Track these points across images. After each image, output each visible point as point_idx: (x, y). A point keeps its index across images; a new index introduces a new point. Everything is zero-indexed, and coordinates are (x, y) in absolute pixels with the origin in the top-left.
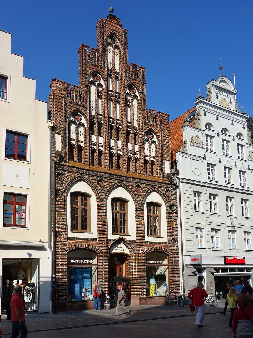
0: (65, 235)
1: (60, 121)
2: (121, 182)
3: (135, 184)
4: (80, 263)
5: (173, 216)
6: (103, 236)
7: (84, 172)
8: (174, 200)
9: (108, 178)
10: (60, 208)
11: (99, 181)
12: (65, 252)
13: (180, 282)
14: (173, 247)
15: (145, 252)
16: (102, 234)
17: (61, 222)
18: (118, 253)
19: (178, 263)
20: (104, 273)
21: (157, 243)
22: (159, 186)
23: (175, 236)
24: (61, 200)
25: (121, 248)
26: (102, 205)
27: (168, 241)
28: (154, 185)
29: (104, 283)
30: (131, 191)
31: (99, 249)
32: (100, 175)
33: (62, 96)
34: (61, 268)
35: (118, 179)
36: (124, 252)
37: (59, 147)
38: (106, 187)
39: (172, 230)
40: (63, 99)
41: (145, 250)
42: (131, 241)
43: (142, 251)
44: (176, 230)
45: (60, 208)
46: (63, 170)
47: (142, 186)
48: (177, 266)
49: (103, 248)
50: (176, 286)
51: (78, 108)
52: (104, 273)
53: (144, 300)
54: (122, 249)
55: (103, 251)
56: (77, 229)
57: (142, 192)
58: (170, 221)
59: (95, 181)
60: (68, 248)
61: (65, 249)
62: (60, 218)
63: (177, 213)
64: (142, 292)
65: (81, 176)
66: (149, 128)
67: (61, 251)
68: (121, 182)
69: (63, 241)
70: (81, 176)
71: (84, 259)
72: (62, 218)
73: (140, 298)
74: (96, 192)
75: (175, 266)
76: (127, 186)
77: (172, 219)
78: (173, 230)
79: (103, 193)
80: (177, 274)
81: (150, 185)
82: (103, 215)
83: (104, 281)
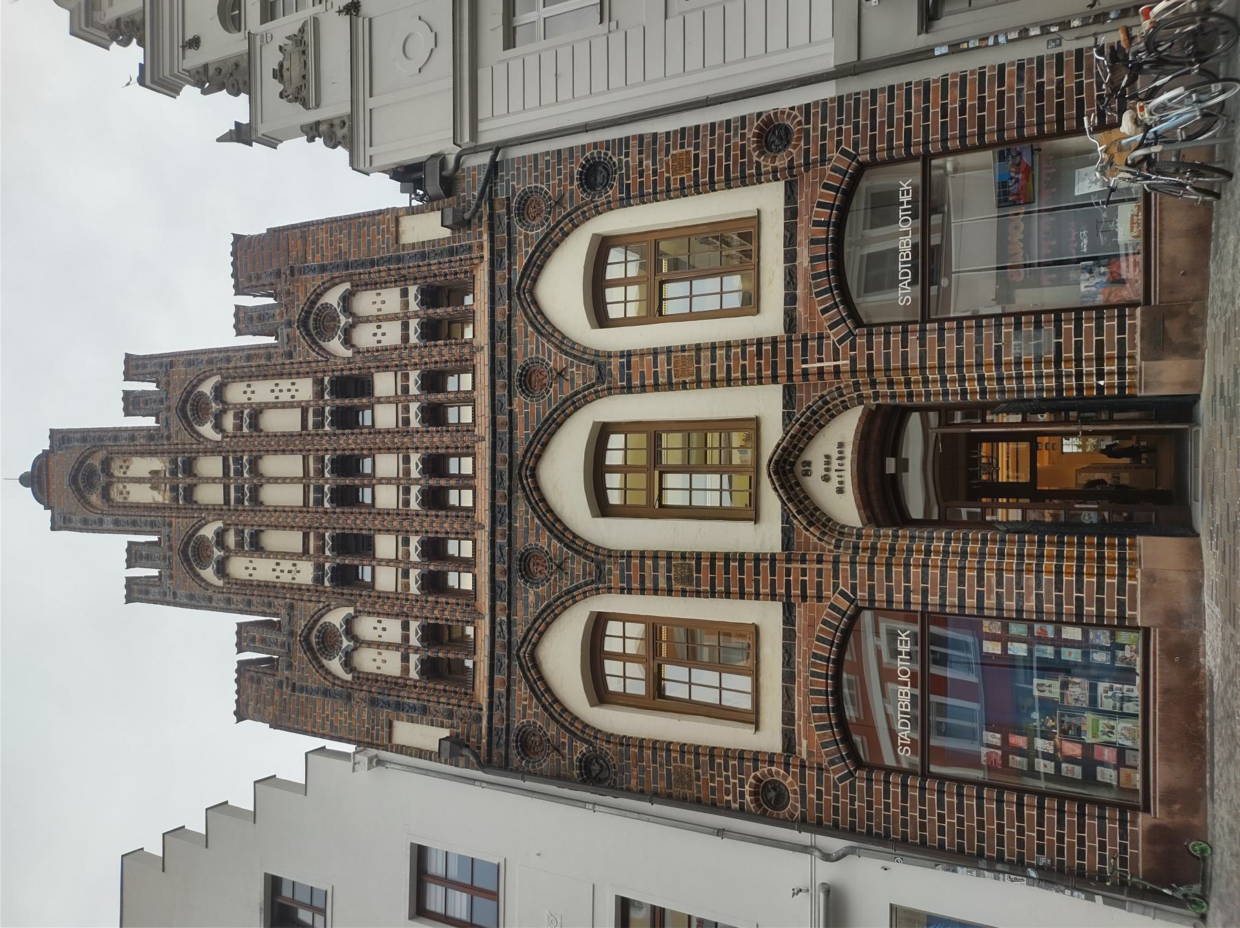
0: (774, 769)
1: (350, 715)
2: (520, 474)
3: (519, 399)
6: (765, 577)
11: (528, 576)
12: (852, 785)
14: (807, 142)
15: (842, 330)
16: (757, 582)
17: (712, 776)
18: (862, 433)
19: (908, 91)
20: (971, 586)
21: (790, 256)
23: (743, 135)
26: (622, 571)
27: (777, 180)
28: (510, 298)
29: (1029, 587)
31: (833, 607)
32: (503, 387)
34: (941, 818)
37: (429, 736)
38: (549, 546)
41: (833, 336)
42: (788, 417)
43: (836, 351)
48: (927, 99)
49: (827, 580)
50: (1070, 84)
52: (971, 586)
54: (835, 455)
58: (668, 179)
59: (531, 598)
60: (832, 763)
61: (841, 779)
67: (853, 800)
68: (520, 474)
69: (803, 780)
70: (518, 657)
72: (697, 767)
74: (574, 404)
75: (926, 110)
77: (655, 172)
78: (712, 153)
80: (982, 90)
82: (669, 570)
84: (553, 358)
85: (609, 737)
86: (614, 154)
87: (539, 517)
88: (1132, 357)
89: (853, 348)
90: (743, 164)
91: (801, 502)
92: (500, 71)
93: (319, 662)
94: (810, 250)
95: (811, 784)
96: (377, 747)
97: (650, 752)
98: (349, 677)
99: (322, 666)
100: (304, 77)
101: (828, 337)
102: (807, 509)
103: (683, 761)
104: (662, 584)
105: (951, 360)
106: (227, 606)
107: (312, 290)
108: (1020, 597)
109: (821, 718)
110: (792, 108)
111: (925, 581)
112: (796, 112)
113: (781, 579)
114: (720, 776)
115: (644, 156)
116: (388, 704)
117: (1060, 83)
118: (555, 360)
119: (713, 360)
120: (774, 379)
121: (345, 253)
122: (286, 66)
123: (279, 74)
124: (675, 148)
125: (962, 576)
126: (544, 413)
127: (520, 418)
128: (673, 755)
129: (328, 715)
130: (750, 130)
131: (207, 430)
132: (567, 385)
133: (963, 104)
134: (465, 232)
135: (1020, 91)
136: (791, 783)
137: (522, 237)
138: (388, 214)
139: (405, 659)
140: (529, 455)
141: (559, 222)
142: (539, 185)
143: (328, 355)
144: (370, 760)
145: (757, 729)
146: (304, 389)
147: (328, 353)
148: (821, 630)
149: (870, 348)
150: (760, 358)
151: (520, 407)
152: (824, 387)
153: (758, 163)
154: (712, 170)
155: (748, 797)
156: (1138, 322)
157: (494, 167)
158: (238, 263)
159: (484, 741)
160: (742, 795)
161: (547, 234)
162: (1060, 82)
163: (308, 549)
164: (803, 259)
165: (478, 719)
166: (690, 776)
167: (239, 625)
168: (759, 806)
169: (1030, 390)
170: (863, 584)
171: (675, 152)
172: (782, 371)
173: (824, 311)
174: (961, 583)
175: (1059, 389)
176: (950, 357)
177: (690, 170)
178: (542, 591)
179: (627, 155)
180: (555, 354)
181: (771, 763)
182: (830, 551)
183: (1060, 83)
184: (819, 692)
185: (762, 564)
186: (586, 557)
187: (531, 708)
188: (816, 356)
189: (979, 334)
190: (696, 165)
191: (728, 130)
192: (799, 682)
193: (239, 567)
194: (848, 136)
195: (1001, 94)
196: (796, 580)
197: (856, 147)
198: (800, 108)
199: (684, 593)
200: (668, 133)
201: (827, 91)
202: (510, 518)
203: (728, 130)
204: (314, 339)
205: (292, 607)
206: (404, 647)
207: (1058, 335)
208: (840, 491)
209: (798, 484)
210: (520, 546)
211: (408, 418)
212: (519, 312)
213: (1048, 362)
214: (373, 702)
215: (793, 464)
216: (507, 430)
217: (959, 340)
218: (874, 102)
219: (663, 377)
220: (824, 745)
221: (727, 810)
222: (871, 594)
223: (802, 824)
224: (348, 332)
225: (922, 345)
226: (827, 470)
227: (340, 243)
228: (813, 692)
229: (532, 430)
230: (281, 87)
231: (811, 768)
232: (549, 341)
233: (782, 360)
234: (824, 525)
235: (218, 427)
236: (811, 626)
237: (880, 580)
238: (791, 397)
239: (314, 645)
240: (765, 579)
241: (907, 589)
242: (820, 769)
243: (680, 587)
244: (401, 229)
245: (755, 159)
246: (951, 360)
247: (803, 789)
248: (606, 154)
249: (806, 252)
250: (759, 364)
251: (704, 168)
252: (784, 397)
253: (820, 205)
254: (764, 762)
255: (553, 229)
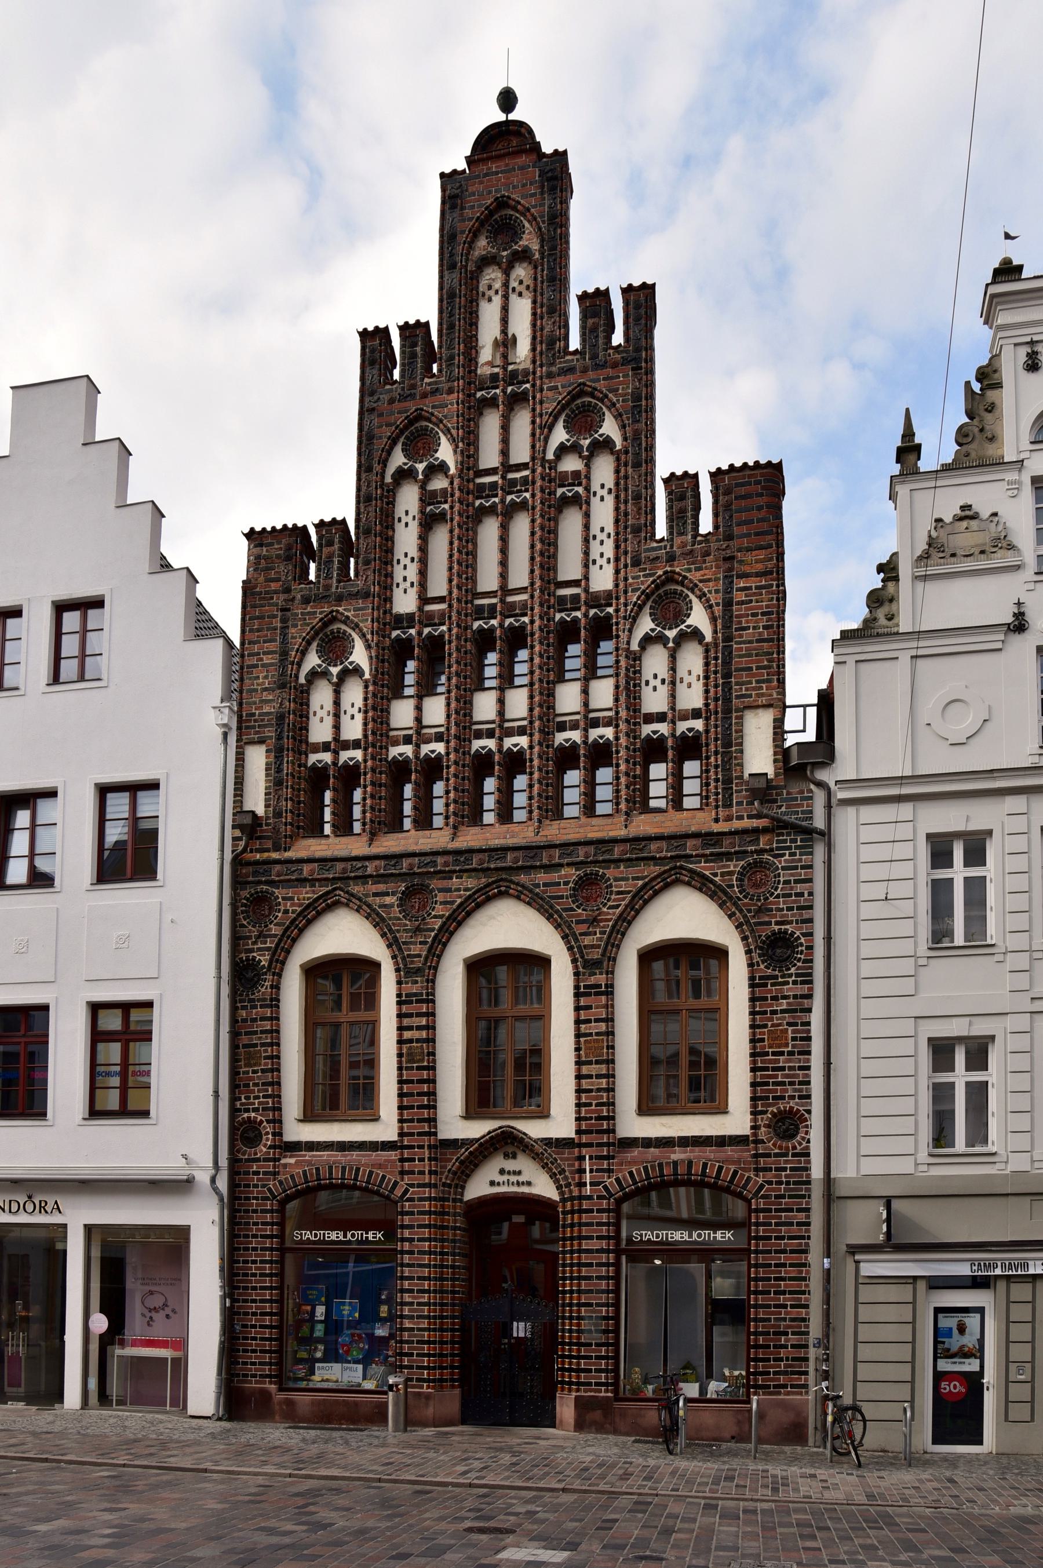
0: (270, 1136)
1: (266, 689)
2: (502, 880)
3: (572, 874)
4: (333, 1242)
5: (785, 997)
6: (417, 1128)
7: (344, 870)
8: (790, 909)
9: (447, 875)
10: (256, 1033)
11: (406, 897)
12: (267, 1199)
13: (807, 1333)
16: (412, 1121)
19: (803, 1238)
21: (685, 1142)
22: (703, 855)
23: (792, 1097)
24: (258, 1000)
25: (519, 1173)
26: (415, 995)
29: (418, 1323)
30: (552, 907)
31: (396, 1183)
33: (274, 586)
35: (489, 869)
36: (536, 1190)
37: (256, 802)
38: (435, 917)
39: (774, 1069)
40: (278, 599)
41: (610, 1181)
42: (548, 1142)
43: (598, 1184)
44: (801, 1068)
45: (256, 1033)
46: (267, 883)
47: (610, 873)
48: (792, 1252)
49: (416, 1179)
51: (332, 611)
52: (417, 1285)
53: (599, 1412)
54: (521, 1179)
55: (768, 1190)
56: (334, 1105)
57: (610, 903)
58: (765, 1026)
59: (388, 900)
60: (281, 1183)
61: (270, 1190)
62: (254, 1072)
63: (807, 979)
64: (590, 1371)
65: (335, 889)
66: (660, 572)
67: (256, 1198)
68: (502, 880)
69: (265, 1160)
70: (335, 889)
71: (344, 1226)
72: (263, 1071)
73: (576, 1397)
75: (784, 1251)
76: (531, 891)
77: (774, 1012)
78: (783, 1069)
79: (421, 943)
80: (791, 1293)
81: (653, 858)
82: (418, 1041)
83: (419, 1317)
84: (610, 911)
85: (276, 987)
86: (799, 968)
87: (461, 904)
88: (578, 1390)
89: (599, 1197)
90: (767, 1098)
91: (481, 1153)
92: (904, 831)
93: (313, 639)
94: (683, 1161)
95: (263, 1167)
96: (239, 728)
97: (269, 1028)
98: (302, 680)
99: (309, 643)
100: (953, 555)
101: (609, 1177)
102: (476, 1157)
103: (266, 1058)
104: (407, 1035)
105: (584, 1271)
106: (363, 499)
107: (706, 590)
108: (412, 1317)
109: (311, 1175)
110: (809, 1141)
111: (419, 1252)
112: (804, 1144)
113: (415, 1141)
114: (259, 1091)
115: (791, 1000)
116: (279, 738)
117: (785, 1347)
118: (608, 914)
119: (599, 1076)
120: (579, 1132)
121: (741, 636)
122: (974, 524)
123: (967, 514)
124: (793, 1032)
125: (424, 1279)
126: (558, 904)
127: (554, 877)
128: (269, 1049)
129: (261, 660)
130: (797, 1104)
131: (560, 435)
132: (583, 928)
133: (783, 1279)
134: (746, 797)
135: (785, 1319)
136: (261, 1151)
137: (732, 868)
138: (778, 693)
139: (326, 747)
140: (519, 888)
141: (741, 911)
142: (780, 886)
143: (634, 619)
144: (225, 725)
145: (300, 1121)
146: (603, 580)
147: (635, 619)
148: (378, 1175)
149: (598, 1211)
150: (597, 1119)
151: (566, 876)
152: (571, 1172)
153: (765, 1112)
154: (766, 1069)
155: (246, 1115)
156: (603, 1394)
157: (809, 833)
158: (748, 472)
159: (258, 856)
160: (247, 1110)
161: (731, 898)
162: (786, 1347)
163: (429, 603)
164: (678, 1155)
165: (277, 848)
166: (255, 1065)
167: (427, 324)
168: (241, 1125)
169: (563, 1324)
170: (415, 1206)
171: (790, 1032)
172: (584, 1139)
173: (631, 1173)
174: (419, 1278)
175: (563, 1344)
176: (586, 1271)
177: (770, 1047)
178: (395, 911)
179: (795, 983)
180: (614, 914)
181: (274, 1134)
182: (441, 1179)
183: (785, 1347)
184: (331, 1173)
185: (426, 1124)
186: (426, 958)
187: (292, 905)
188: (595, 1167)
189: (603, 1292)
190: (774, 1054)
191: (801, 1083)
192: (337, 1156)
193: (408, 499)
194: (774, 1190)
195: (785, 1306)
196: (415, 1154)
197: (763, 1197)
198: (808, 1148)
199: (400, 1055)
200: (809, 1024)
201: (817, 1172)
202: (460, 871)
203: (801, 1083)
204: (653, 593)
205: (366, 595)
206: (339, 744)
207: (597, 1345)
208: (492, 1183)
209: (496, 1149)
210: (435, 884)
211: (564, 730)
212: (657, 869)
213: (578, 1338)
214: (281, 718)
215: (513, 1144)
216: (545, 861)
217: (599, 1278)
218: (799, 1210)
219: (586, 1028)
220: (292, 1177)
221: (233, 1099)
222: (408, 1213)
223: (233, 1161)
224: (661, 639)
225: (598, 1251)
226: (509, 1173)
227: (754, 628)
228: (331, 1168)
229: (543, 891)
230: (948, 519)
231: (274, 1167)
232: (627, 906)
233: (593, 1138)
234: (463, 1172)
235: (563, 450)
236: (380, 1166)
237: (418, 1220)
238: (565, 1145)
239: (331, 628)
240: (414, 1128)
241: (413, 1240)
242: (275, 1174)
243: (404, 1051)
244: (760, 711)
245: (770, 1109)
246: (584, 1271)
247: (258, 1160)
248: (799, 960)
249: (682, 1156)
250: (591, 1118)
251: (770, 1061)
252: (564, 1139)
253: (720, 1168)
254: (274, 1128)
255: (735, 904)
